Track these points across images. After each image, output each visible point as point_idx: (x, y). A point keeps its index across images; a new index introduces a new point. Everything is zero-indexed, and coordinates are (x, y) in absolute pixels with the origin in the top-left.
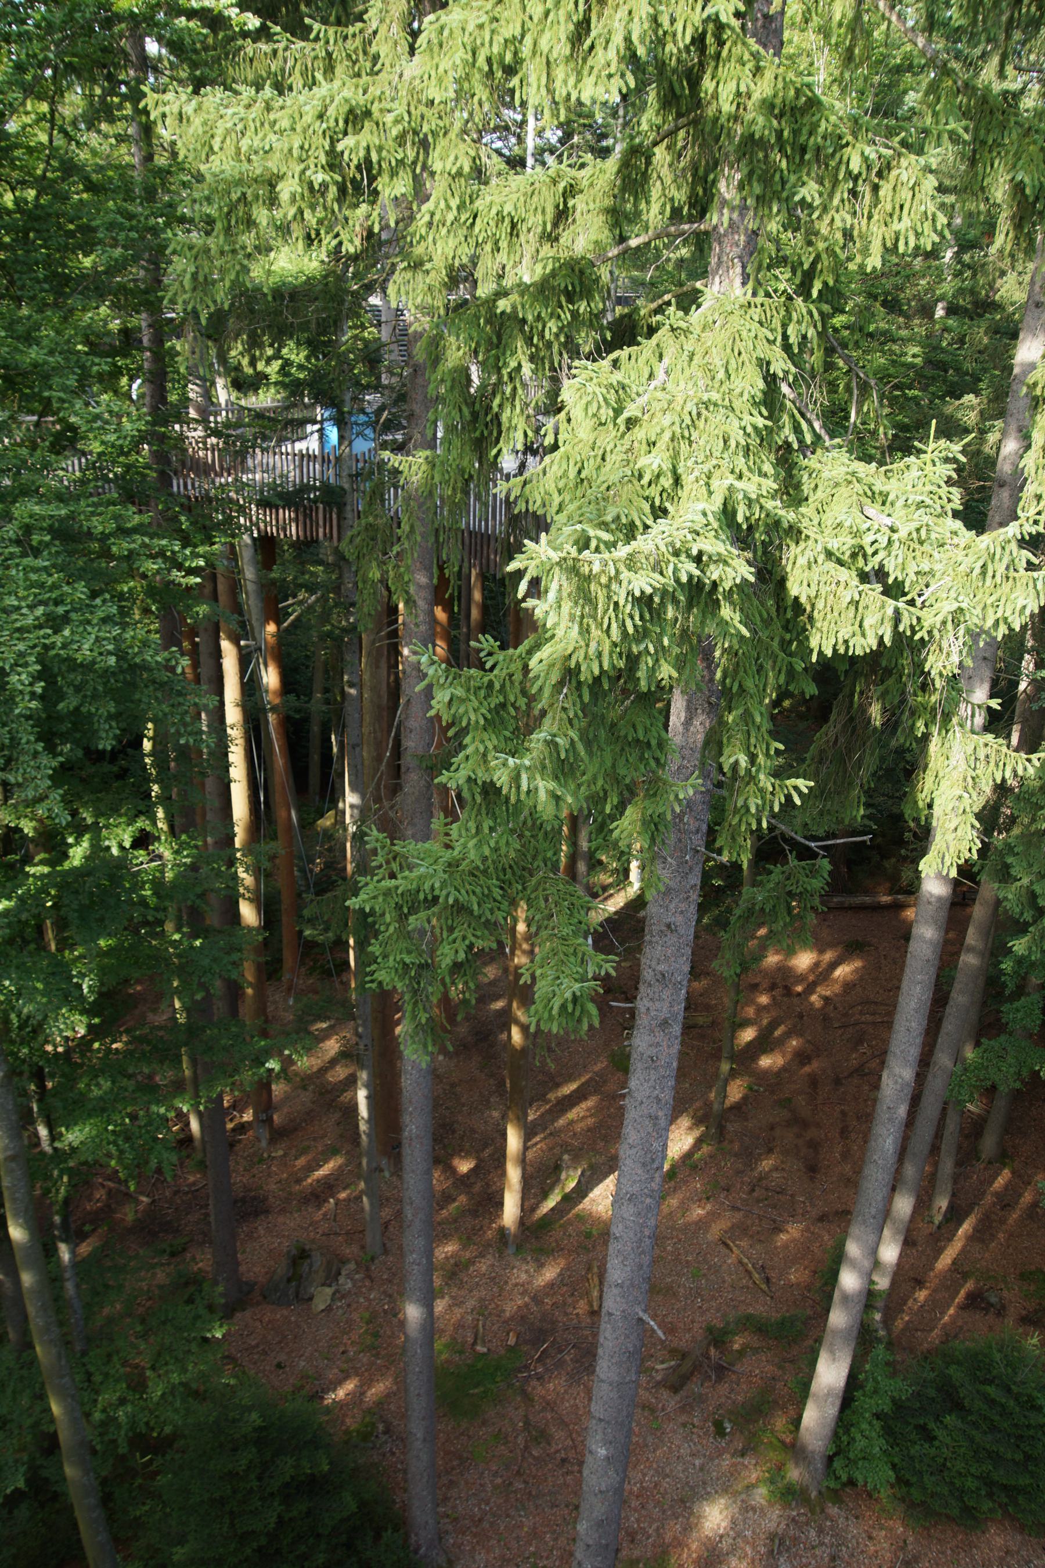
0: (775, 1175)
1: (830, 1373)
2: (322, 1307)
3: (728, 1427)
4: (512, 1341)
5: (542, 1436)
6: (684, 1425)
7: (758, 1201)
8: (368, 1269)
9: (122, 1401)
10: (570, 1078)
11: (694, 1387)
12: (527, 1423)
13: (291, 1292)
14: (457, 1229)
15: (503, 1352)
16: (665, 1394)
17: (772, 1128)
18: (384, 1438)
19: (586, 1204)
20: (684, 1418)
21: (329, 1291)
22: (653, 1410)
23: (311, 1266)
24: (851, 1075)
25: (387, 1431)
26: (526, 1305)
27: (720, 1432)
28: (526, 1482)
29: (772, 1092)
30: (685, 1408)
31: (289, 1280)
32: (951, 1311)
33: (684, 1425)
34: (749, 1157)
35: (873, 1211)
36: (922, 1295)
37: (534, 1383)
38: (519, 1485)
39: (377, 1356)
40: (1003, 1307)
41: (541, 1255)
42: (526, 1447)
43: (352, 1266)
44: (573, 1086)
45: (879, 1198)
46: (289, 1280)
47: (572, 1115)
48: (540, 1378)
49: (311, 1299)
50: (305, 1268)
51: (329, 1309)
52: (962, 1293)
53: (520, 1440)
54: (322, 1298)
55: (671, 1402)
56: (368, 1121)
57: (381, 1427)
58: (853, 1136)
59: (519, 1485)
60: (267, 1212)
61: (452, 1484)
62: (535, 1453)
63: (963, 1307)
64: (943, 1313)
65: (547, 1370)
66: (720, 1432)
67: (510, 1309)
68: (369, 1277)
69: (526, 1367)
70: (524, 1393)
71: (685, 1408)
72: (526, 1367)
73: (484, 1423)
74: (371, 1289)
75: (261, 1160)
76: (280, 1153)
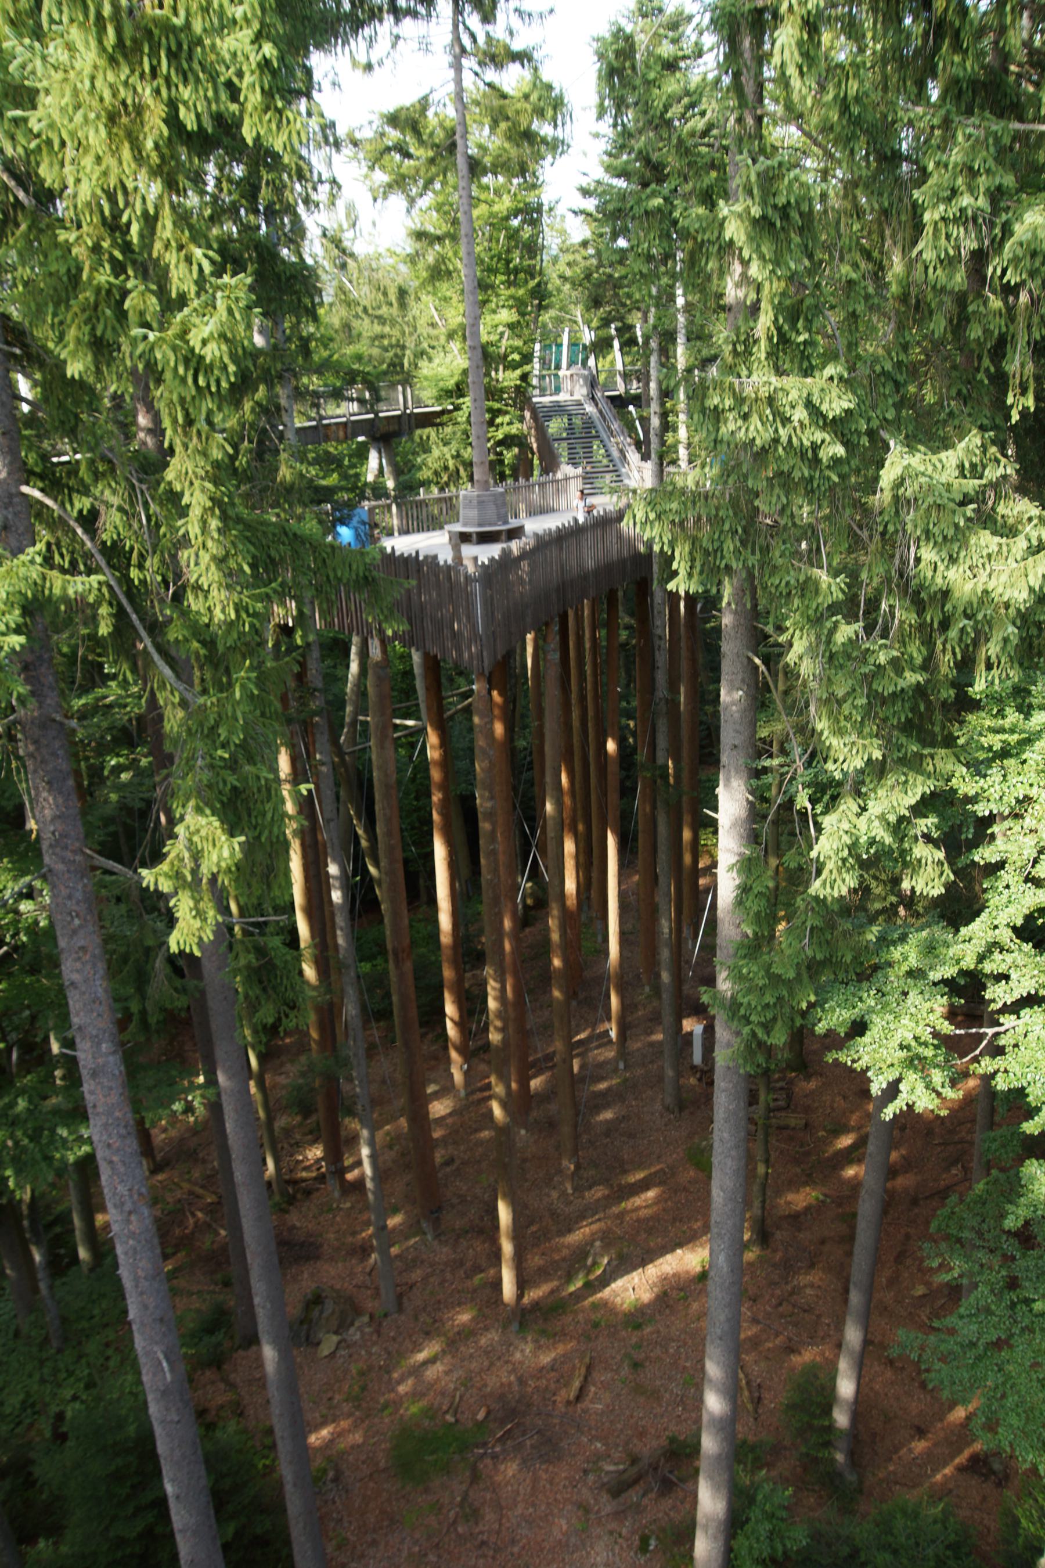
0: (808, 1291)
1: (710, 1502)
2: (326, 1353)
3: (653, 1543)
4: (481, 1416)
5: (474, 1515)
6: (611, 1533)
7: (782, 1316)
8: (380, 1324)
9: (75, 1398)
10: (640, 1166)
11: (633, 1495)
12: (464, 1498)
13: (303, 1334)
14: (472, 1300)
15: (470, 1425)
16: (605, 1497)
17: (823, 1242)
18: (330, 1486)
19: (606, 1293)
20: (613, 1525)
21: (335, 1339)
22: (587, 1511)
23: (321, 1312)
24: (932, 1196)
25: (336, 1480)
26: (510, 1384)
27: (644, 1547)
28: (440, 1557)
29: (840, 1205)
30: (619, 1515)
31: (302, 1322)
32: (947, 1471)
33: (611, 1533)
34: (788, 1268)
35: (719, 1331)
36: (920, 1446)
37: (488, 1461)
38: (432, 1558)
39: (358, 1407)
40: (1007, 1477)
41: (550, 1335)
42: (455, 1522)
43: (366, 1319)
44: (640, 1175)
45: (722, 1318)
46: (302, 1322)
47: (638, 1201)
48: (495, 1457)
49: (318, 1344)
50: (316, 1313)
51: (332, 1355)
52: (966, 1453)
53: (452, 1514)
54: (329, 1343)
55: (607, 1505)
56: (373, 1179)
57: (331, 1474)
58: (908, 1262)
59: (432, 1558)
60: (318, 1258)
61: (374, 1543)
62: (460, 1530)
63: (961, 1469)
64: (935, 1471)
65: (504, 1451)
66: (644, 1547)
67: (492, 1382)
68: (378, 1332)
69: (484, 1444)
70: (474, 1469)
71: (619, 1515)
72: (484, 1444)
73: (427, 1490)
74: (374, 1344)
75: (330, 1210)
76: (348, 1205)
